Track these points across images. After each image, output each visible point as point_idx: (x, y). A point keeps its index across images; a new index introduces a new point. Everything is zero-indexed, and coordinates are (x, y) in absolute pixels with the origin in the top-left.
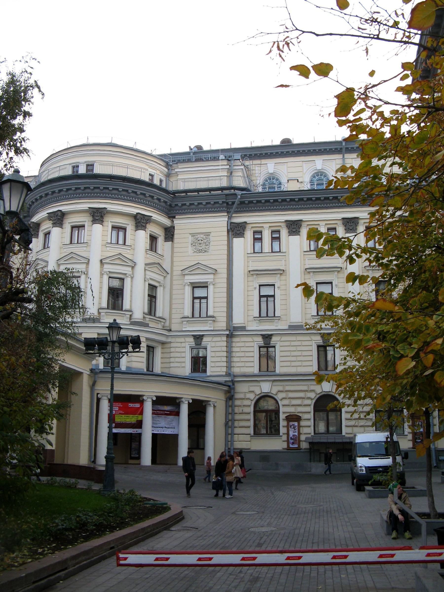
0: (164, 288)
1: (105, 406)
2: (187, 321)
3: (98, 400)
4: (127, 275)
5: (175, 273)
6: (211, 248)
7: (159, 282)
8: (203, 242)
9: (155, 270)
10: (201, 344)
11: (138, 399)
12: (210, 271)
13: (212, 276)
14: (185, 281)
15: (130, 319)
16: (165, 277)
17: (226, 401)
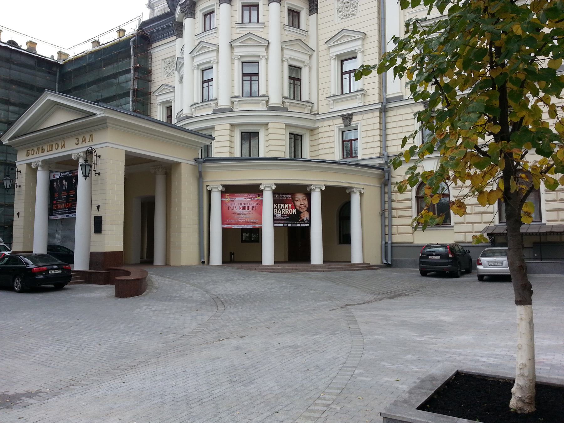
0: (310, 68)
1: (216, 197)
2: (334, 101)
3: (209, 193)
4: (261, 57)
5: (320, 49)
6: (360, 8)
7: (303, 62)
8: (349, 4)
9: (297, 48)
10: (350, 124)
11: (255, 190)
12: (357, 36)
13: (360, 42)
14: (331, 55)
15: (267, 106)
16: (311, 56)
17: (381, 187)
